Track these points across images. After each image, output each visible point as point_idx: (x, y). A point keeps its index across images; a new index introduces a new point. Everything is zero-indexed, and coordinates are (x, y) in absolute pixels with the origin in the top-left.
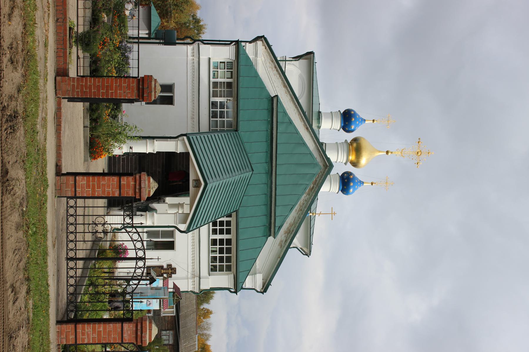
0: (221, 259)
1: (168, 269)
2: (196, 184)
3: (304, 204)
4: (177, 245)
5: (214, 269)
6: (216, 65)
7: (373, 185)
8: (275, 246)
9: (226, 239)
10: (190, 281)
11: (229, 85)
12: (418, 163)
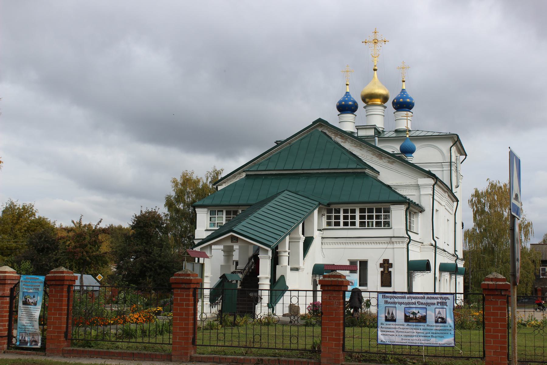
0: (378, 217)
1: (384, 267)
2: (235, 240)
3: (355, 143)
4: (363, 258)
5: (387, 224)
6: (213, 224)
7: (404, 80)
8: (393, 168)
9: (360, 213)
10: (396, 246)
11: (228, 213)
12: (385, 42)
